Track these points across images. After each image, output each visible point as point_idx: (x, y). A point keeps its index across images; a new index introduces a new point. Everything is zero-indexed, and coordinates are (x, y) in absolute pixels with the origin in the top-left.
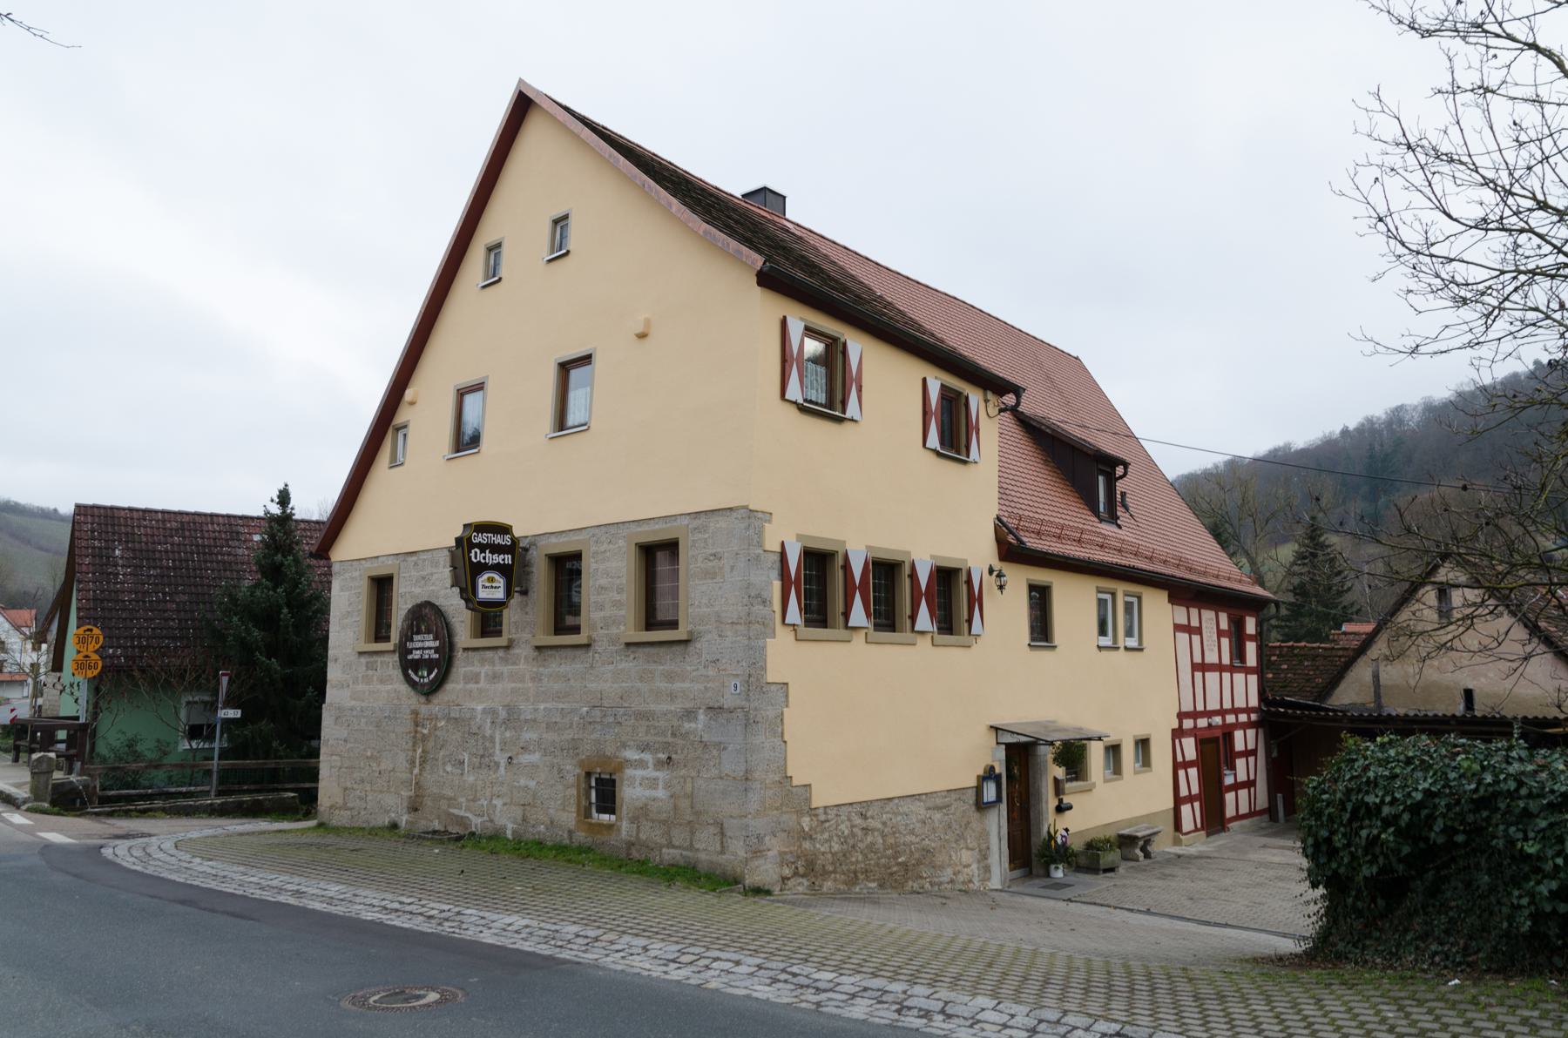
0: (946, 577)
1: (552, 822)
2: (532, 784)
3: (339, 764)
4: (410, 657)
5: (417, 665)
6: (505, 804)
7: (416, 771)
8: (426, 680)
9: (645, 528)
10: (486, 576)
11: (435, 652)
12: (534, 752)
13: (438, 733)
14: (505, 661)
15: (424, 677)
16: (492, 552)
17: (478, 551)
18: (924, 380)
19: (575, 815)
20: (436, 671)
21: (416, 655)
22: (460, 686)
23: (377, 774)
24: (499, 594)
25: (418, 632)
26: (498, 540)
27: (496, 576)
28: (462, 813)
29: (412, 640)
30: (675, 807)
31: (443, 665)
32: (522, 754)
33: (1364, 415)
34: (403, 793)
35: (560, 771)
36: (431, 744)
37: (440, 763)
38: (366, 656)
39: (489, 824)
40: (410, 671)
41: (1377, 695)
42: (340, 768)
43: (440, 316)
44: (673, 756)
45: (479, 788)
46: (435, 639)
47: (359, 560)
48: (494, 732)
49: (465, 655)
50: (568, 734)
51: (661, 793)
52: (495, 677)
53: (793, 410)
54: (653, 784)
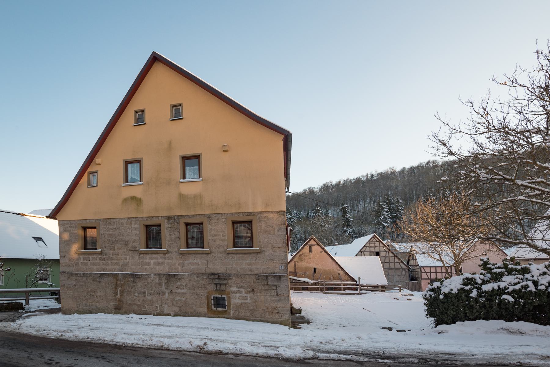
7: (118, 296)
33: (304, 189)
35: (197, 294)
41: (295, 269)
43: (136, 93)
44: (255, 289)
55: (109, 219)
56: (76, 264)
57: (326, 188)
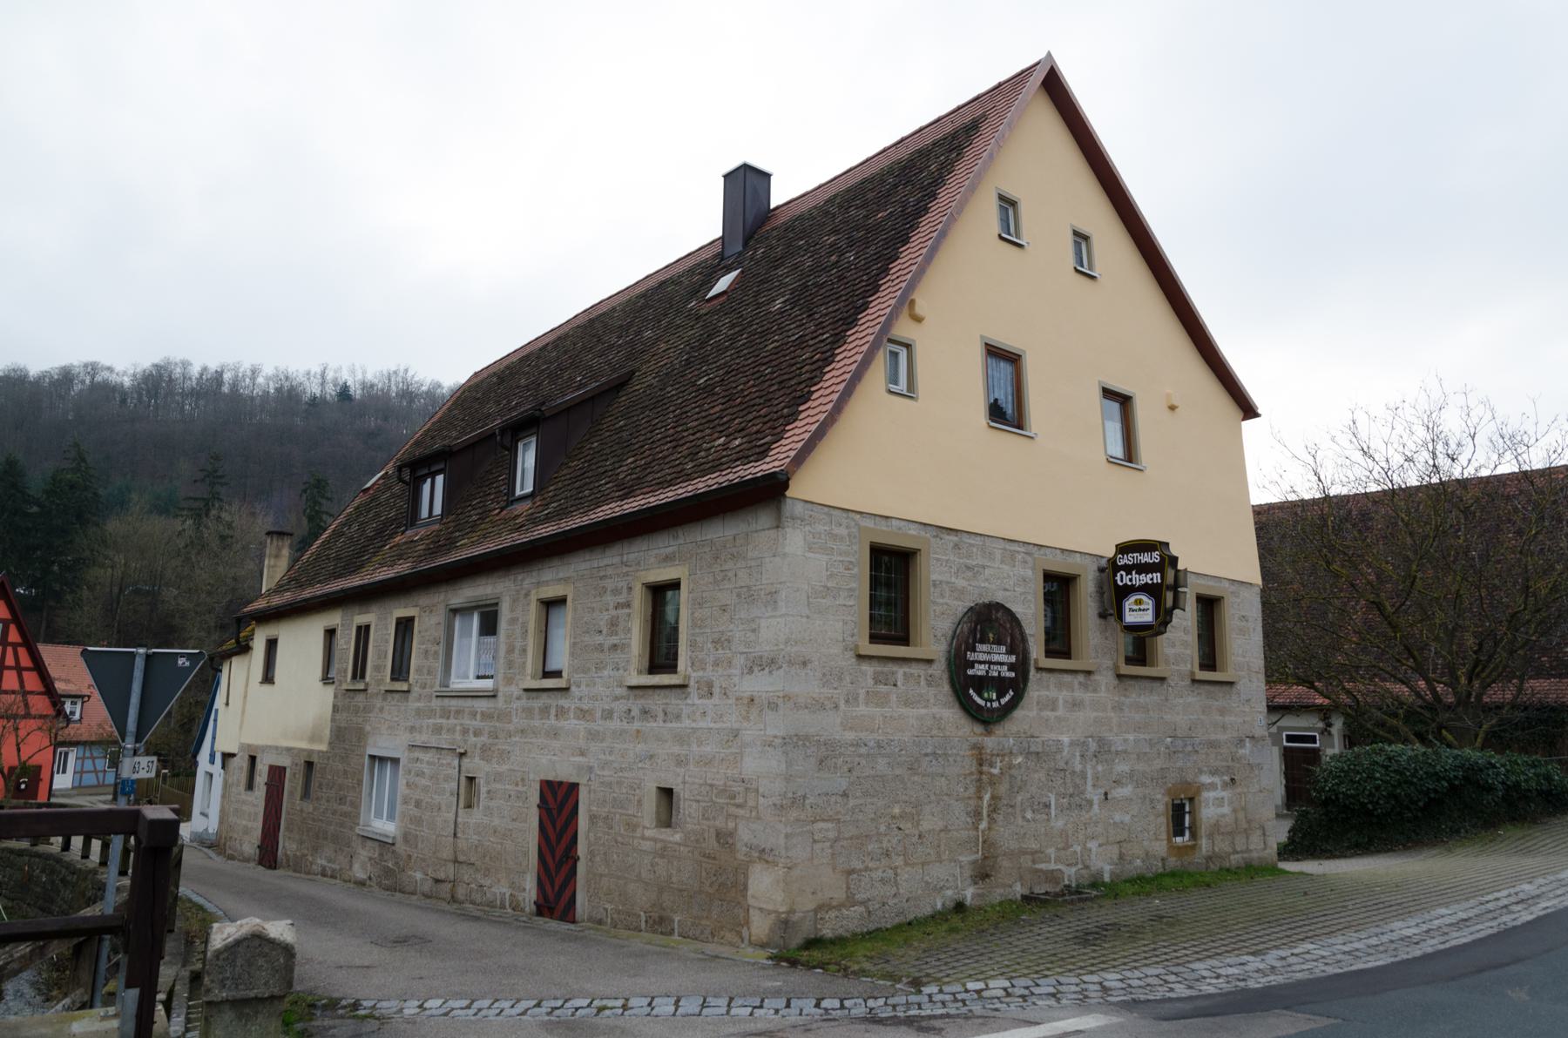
1: (1147, 854)
2: (1127, 818)
3: (832, 835)
4: (970, 672)
5: (981, 684)
6: (1100, 845)
7: (983, 825)
8: (995, 705)
9: (1211, 583)
10: (1132, 599)
11: (1009, 670)
12: (1127, 785)
13: (1013, 772)
14: (1084, 686)
15: (991, 701)
16: (1139, 573)
17: (1123, 573)
19: (1165, 842)
20: (1011, 693)
21: (980, 670)
22: (1033, 714)
23: (915, 840)
24: (1148, 617)
25: (982, 641)
26: (1145, 558)
27: (1144, 598)
28: (1052, 866)
29: (974, 650)
30: (1236, 819)
31: (1015, 685)
32: (1115, 788)
33: (63, 363)
34: (961, 858)
35: (1152, 801)
36: (1003, 789)
37: (1018, 810)
38: (875, 662)
39: (1084, 872)
40: (971, 691)
42: (836, 840)
43: (1203, 360)
45: (1070, 832)
46: (1010, 652)
47: (875, 515)
48: (1085, 767)
49: (1039, 676)
50: (1158, 764)
51: (1226, 810)
52: (1076, 705)
54: (1220, 802)
55: (957, 531)
56: (847, 701)
57: (157, 383)
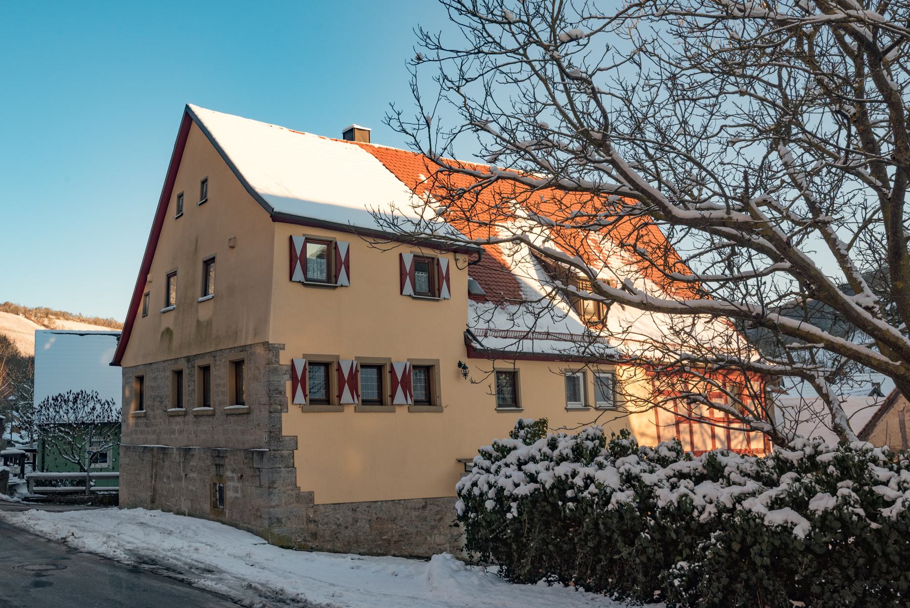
0: (427, 371)
18: (401, 255)
53: (300, 286)
